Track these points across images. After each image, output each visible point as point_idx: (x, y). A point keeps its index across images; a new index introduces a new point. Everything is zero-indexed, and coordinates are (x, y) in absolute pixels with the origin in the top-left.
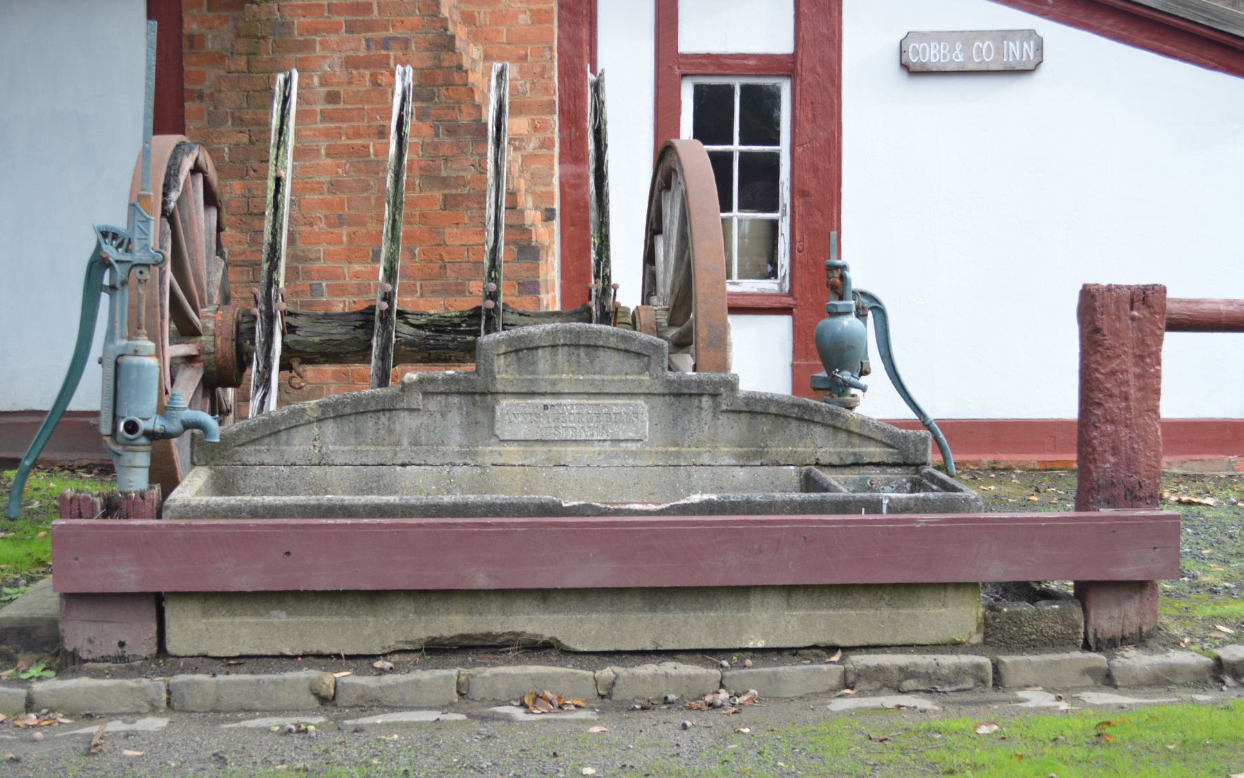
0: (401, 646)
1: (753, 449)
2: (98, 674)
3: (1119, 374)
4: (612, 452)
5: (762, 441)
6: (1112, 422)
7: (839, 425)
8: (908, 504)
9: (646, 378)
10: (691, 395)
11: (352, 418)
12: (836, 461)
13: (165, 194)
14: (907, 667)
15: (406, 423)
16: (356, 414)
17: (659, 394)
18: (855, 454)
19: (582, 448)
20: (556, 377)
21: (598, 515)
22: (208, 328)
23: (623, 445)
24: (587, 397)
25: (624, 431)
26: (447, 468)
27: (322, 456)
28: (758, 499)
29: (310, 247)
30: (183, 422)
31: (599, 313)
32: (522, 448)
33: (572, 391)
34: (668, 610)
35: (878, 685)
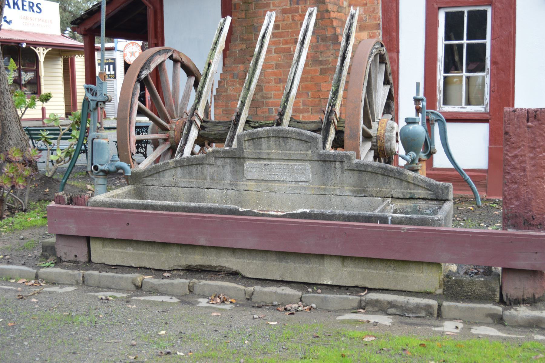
0: (176, 267)
1: (360, 188)
2: (69, 268)
3: (520, 157)
4: (295, 187)
5: (365, 185)
6: (516, 183)
7: (402, 178)
8: (401, 220)
9: (309, 152)
10: (331, 161)
11: (187, 167)
12: (402, 196)
13: (141, 72)
14: (392, 302)
15: (208, 170)
16: (189, 165)
17: (316, 161)
18: (411, 193)
19: (282, 185)
20: (270, 151)
21: (254, 216)
22: (172, 127)
23: (300, 184)
24: (284, 161)
25: (300, 177)
26: (225, 191)
27: (176, 183)
28: (327, 213)
29: (268, 92)
30: (116, 167)
31: (326, 122)
32: (256, 183)
33: (277, 158)
34: (287, 262)
35: (377, 309)
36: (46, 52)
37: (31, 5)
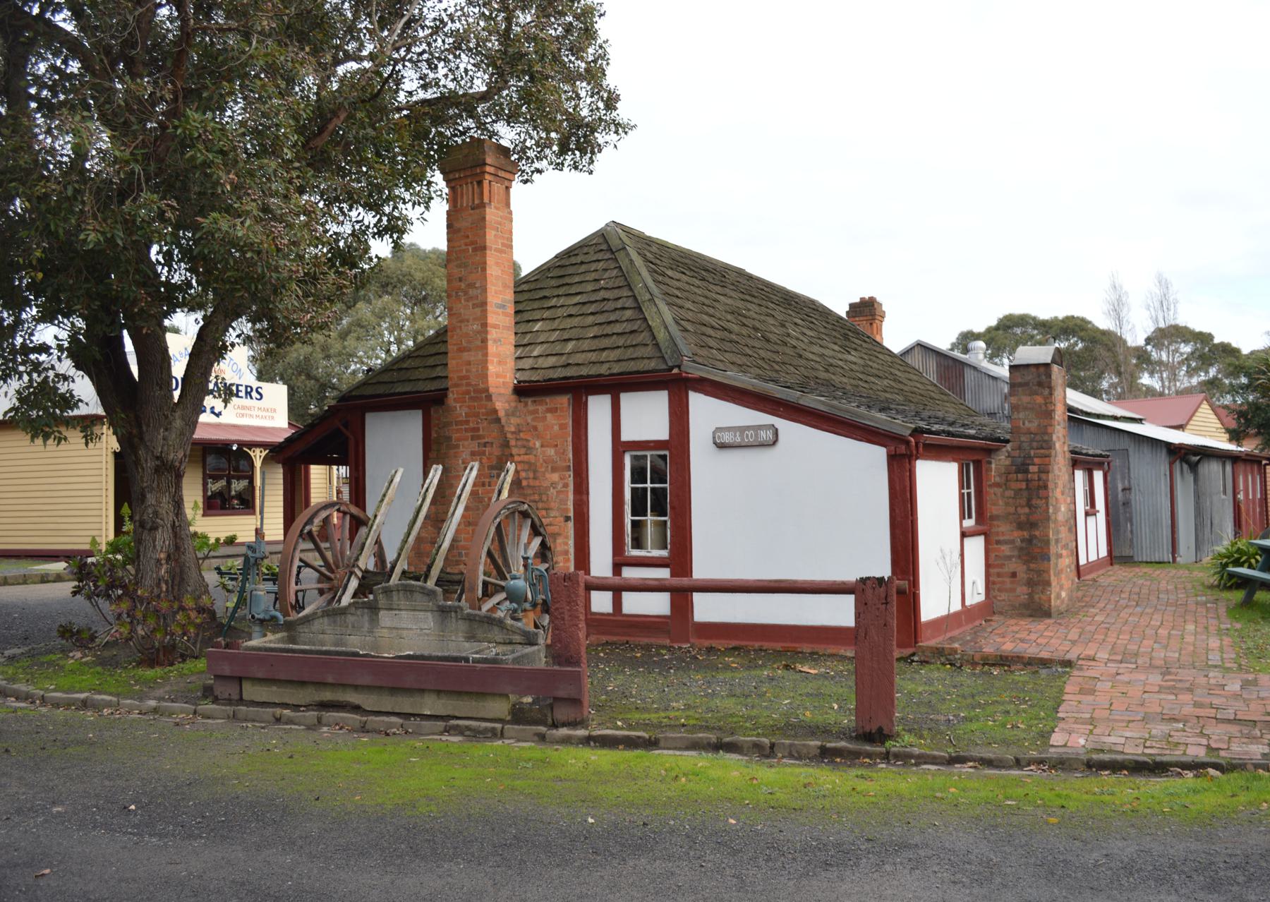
2: (223, 705)
13: (304, 527)
15: (350, 619)
36: (264, 454)
37: (249, 389)
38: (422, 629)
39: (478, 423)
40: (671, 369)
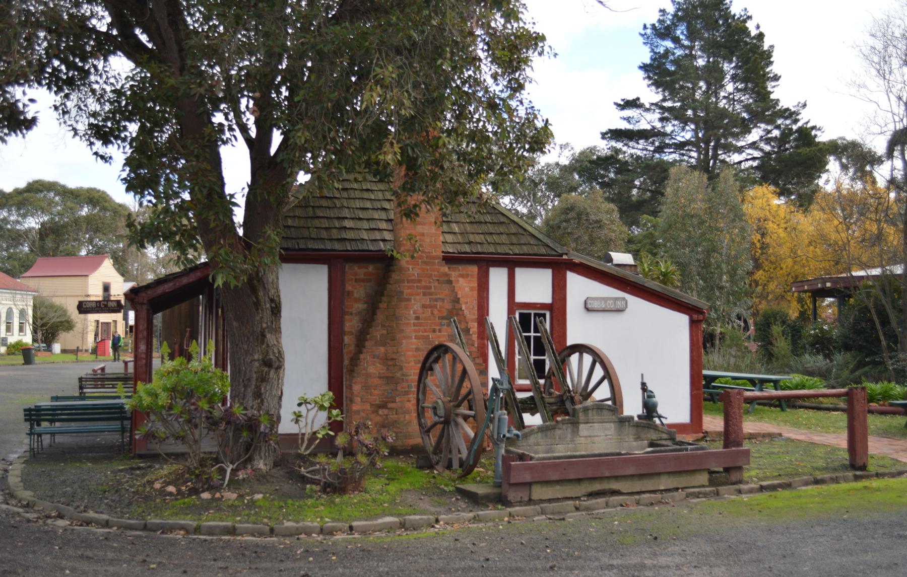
15: (558, 432)
38: (606, 435)
39: (430, 282)
40: (561, 255)
